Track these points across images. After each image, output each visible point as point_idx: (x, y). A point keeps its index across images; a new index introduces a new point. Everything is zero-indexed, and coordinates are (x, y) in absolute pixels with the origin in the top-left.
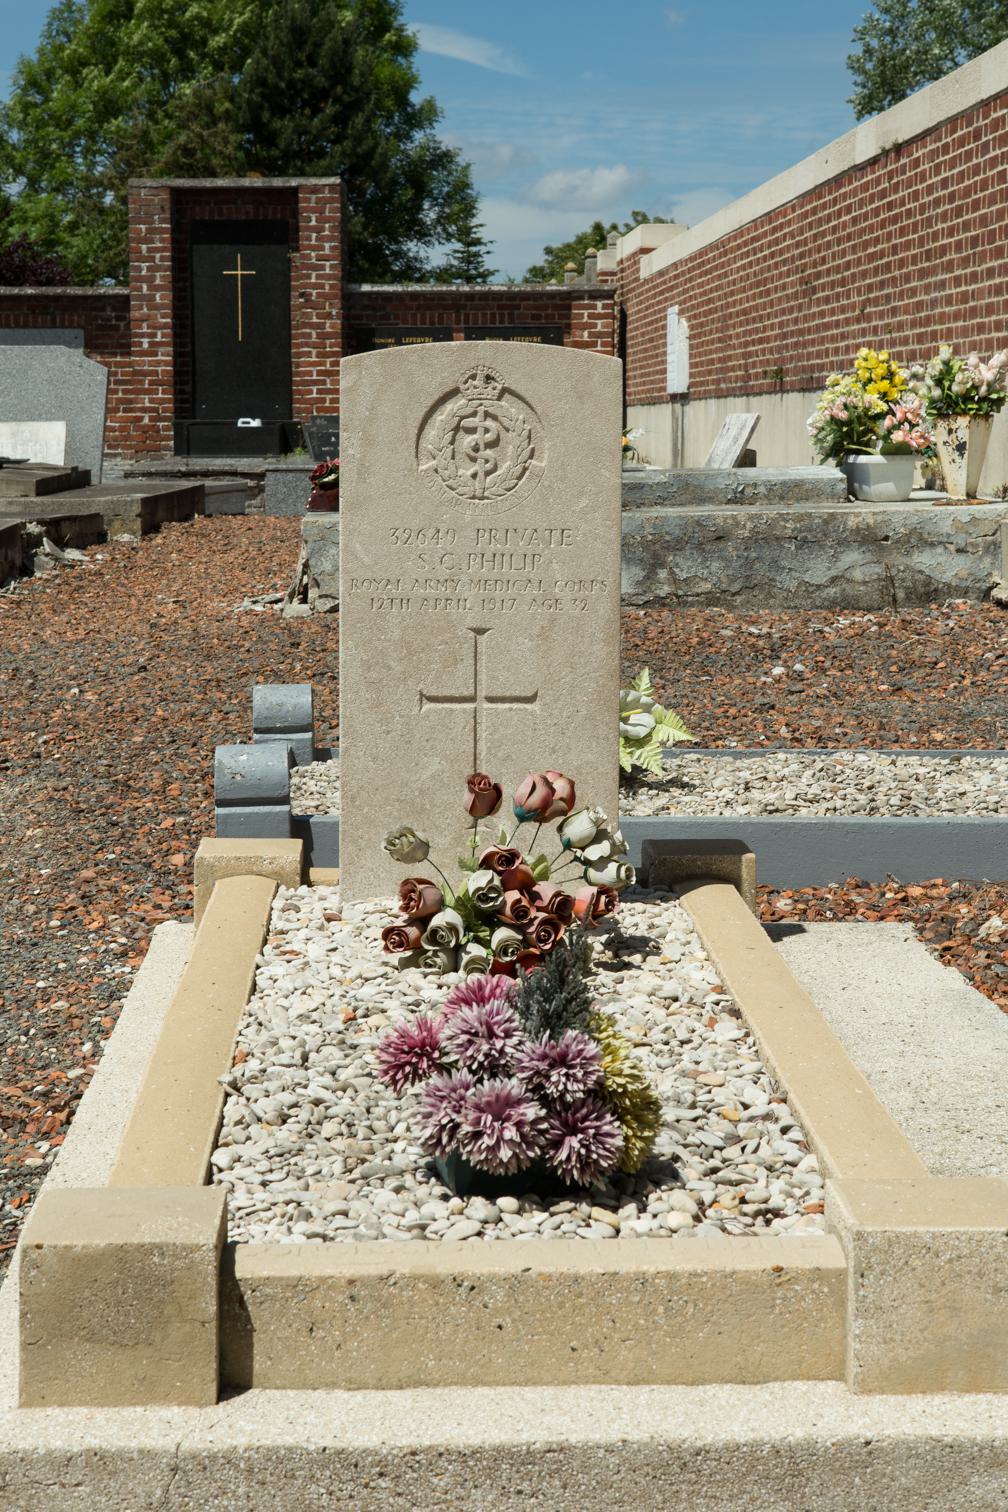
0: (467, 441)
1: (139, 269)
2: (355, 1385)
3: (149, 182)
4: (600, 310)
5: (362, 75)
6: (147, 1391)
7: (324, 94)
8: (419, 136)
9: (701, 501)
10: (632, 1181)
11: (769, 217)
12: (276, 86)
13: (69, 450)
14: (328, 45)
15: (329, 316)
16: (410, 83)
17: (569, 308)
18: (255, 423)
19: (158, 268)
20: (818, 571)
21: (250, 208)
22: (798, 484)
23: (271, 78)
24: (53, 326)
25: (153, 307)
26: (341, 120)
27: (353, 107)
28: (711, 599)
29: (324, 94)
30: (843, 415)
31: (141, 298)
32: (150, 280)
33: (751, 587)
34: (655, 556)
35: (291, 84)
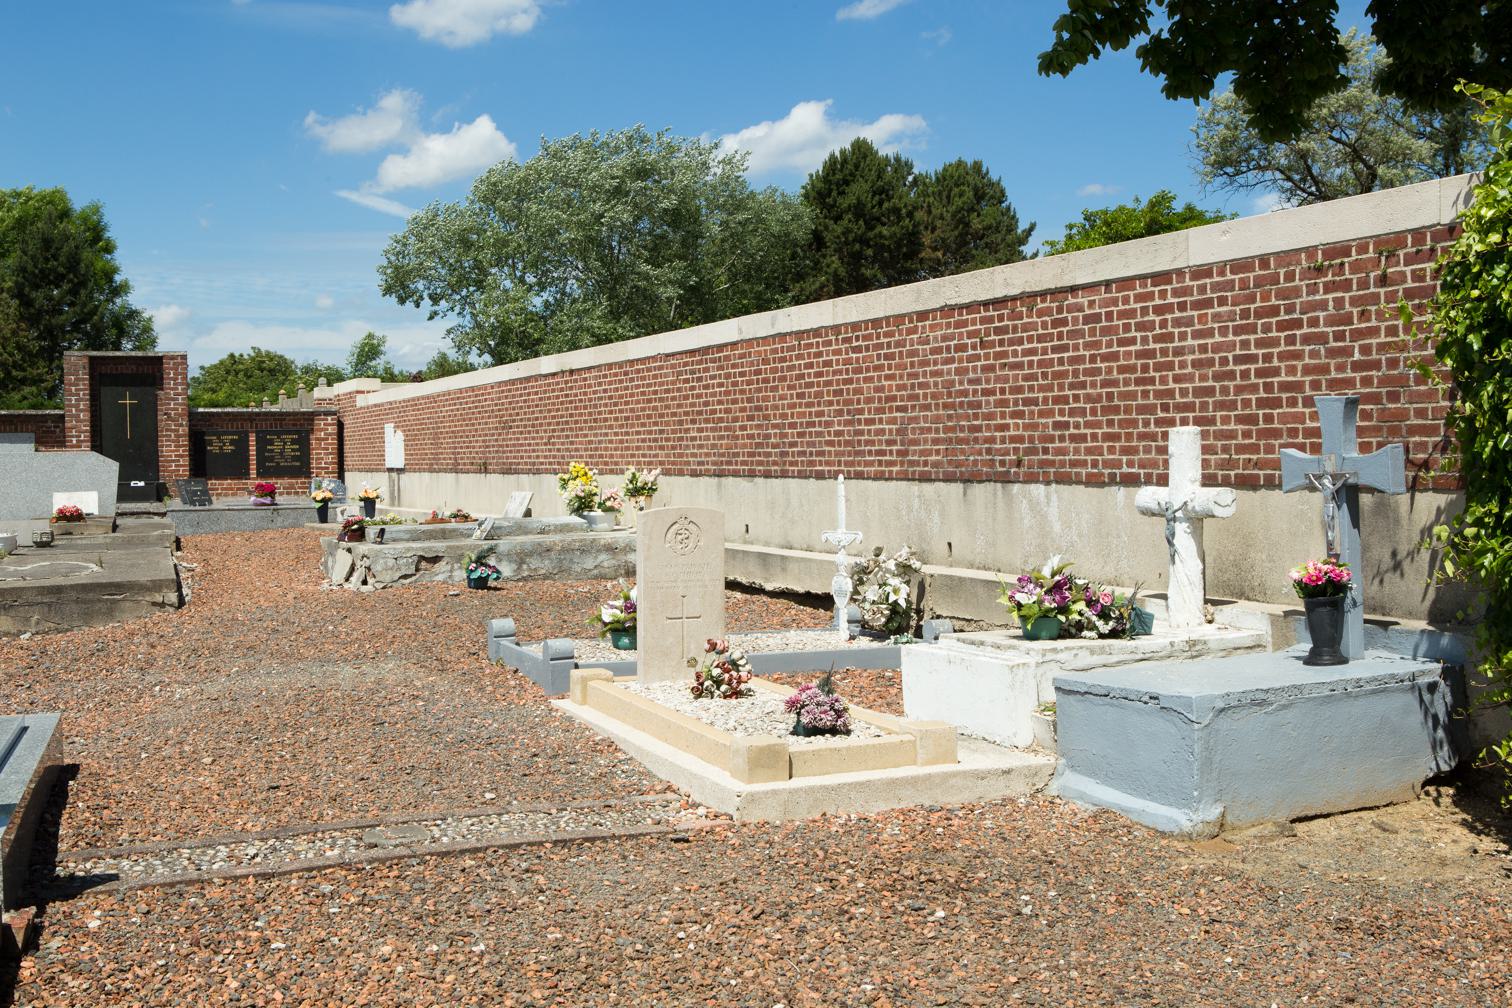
0: (680, 537)
1: (70, 400)
2: (815, 775)
3: (76, 353)
4: (330, 421)
5: (87, 267)
6: (775, 779)
7: (62, 277)
8: (118, 301)
9: (526, 533)
10: (848, 732)
11: (472, 389)
12: (33, 273)
13: (100, 507)
14: (65, 249)
15: (181, 425)
16: (115, 270)
17: (313, 420)
18: (142, 484)
19: (82, 400)
20: (589, 563)
21: (134, 367)
22: (567, 525)
23: (30, 267)
24: (16, 431)
25: (79, 420)
26: (74, 292)
27: (83, 284)
28: (545, 577)
29: (62, 277)
30: (582, 494)
31: (72, 416)
32: (77, 406)
33: (562, 571)
34: (521, 559)
35: (42, 271)
